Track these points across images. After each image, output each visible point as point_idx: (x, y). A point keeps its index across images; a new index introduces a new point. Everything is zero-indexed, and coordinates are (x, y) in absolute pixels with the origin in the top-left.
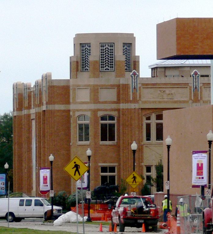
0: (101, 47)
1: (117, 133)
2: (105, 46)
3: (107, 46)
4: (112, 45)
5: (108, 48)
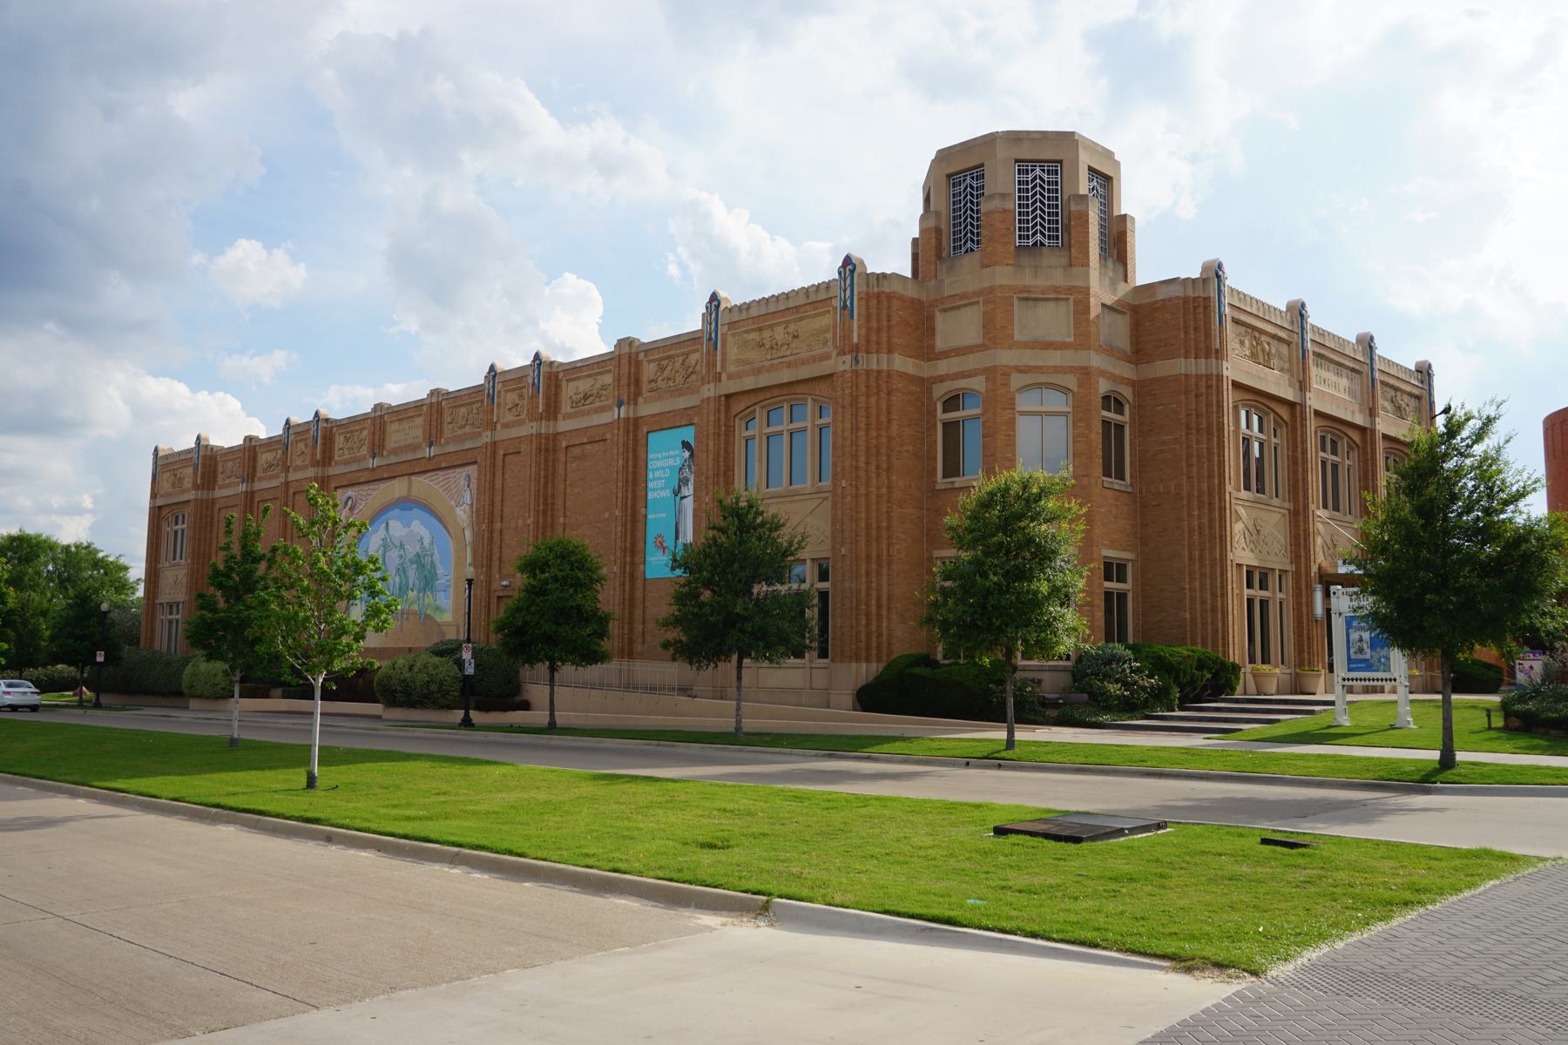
0: (1019, 174)
1: (936, 449)
2: (1032, 170)
3: (968, 180)
5: (1041, 179)
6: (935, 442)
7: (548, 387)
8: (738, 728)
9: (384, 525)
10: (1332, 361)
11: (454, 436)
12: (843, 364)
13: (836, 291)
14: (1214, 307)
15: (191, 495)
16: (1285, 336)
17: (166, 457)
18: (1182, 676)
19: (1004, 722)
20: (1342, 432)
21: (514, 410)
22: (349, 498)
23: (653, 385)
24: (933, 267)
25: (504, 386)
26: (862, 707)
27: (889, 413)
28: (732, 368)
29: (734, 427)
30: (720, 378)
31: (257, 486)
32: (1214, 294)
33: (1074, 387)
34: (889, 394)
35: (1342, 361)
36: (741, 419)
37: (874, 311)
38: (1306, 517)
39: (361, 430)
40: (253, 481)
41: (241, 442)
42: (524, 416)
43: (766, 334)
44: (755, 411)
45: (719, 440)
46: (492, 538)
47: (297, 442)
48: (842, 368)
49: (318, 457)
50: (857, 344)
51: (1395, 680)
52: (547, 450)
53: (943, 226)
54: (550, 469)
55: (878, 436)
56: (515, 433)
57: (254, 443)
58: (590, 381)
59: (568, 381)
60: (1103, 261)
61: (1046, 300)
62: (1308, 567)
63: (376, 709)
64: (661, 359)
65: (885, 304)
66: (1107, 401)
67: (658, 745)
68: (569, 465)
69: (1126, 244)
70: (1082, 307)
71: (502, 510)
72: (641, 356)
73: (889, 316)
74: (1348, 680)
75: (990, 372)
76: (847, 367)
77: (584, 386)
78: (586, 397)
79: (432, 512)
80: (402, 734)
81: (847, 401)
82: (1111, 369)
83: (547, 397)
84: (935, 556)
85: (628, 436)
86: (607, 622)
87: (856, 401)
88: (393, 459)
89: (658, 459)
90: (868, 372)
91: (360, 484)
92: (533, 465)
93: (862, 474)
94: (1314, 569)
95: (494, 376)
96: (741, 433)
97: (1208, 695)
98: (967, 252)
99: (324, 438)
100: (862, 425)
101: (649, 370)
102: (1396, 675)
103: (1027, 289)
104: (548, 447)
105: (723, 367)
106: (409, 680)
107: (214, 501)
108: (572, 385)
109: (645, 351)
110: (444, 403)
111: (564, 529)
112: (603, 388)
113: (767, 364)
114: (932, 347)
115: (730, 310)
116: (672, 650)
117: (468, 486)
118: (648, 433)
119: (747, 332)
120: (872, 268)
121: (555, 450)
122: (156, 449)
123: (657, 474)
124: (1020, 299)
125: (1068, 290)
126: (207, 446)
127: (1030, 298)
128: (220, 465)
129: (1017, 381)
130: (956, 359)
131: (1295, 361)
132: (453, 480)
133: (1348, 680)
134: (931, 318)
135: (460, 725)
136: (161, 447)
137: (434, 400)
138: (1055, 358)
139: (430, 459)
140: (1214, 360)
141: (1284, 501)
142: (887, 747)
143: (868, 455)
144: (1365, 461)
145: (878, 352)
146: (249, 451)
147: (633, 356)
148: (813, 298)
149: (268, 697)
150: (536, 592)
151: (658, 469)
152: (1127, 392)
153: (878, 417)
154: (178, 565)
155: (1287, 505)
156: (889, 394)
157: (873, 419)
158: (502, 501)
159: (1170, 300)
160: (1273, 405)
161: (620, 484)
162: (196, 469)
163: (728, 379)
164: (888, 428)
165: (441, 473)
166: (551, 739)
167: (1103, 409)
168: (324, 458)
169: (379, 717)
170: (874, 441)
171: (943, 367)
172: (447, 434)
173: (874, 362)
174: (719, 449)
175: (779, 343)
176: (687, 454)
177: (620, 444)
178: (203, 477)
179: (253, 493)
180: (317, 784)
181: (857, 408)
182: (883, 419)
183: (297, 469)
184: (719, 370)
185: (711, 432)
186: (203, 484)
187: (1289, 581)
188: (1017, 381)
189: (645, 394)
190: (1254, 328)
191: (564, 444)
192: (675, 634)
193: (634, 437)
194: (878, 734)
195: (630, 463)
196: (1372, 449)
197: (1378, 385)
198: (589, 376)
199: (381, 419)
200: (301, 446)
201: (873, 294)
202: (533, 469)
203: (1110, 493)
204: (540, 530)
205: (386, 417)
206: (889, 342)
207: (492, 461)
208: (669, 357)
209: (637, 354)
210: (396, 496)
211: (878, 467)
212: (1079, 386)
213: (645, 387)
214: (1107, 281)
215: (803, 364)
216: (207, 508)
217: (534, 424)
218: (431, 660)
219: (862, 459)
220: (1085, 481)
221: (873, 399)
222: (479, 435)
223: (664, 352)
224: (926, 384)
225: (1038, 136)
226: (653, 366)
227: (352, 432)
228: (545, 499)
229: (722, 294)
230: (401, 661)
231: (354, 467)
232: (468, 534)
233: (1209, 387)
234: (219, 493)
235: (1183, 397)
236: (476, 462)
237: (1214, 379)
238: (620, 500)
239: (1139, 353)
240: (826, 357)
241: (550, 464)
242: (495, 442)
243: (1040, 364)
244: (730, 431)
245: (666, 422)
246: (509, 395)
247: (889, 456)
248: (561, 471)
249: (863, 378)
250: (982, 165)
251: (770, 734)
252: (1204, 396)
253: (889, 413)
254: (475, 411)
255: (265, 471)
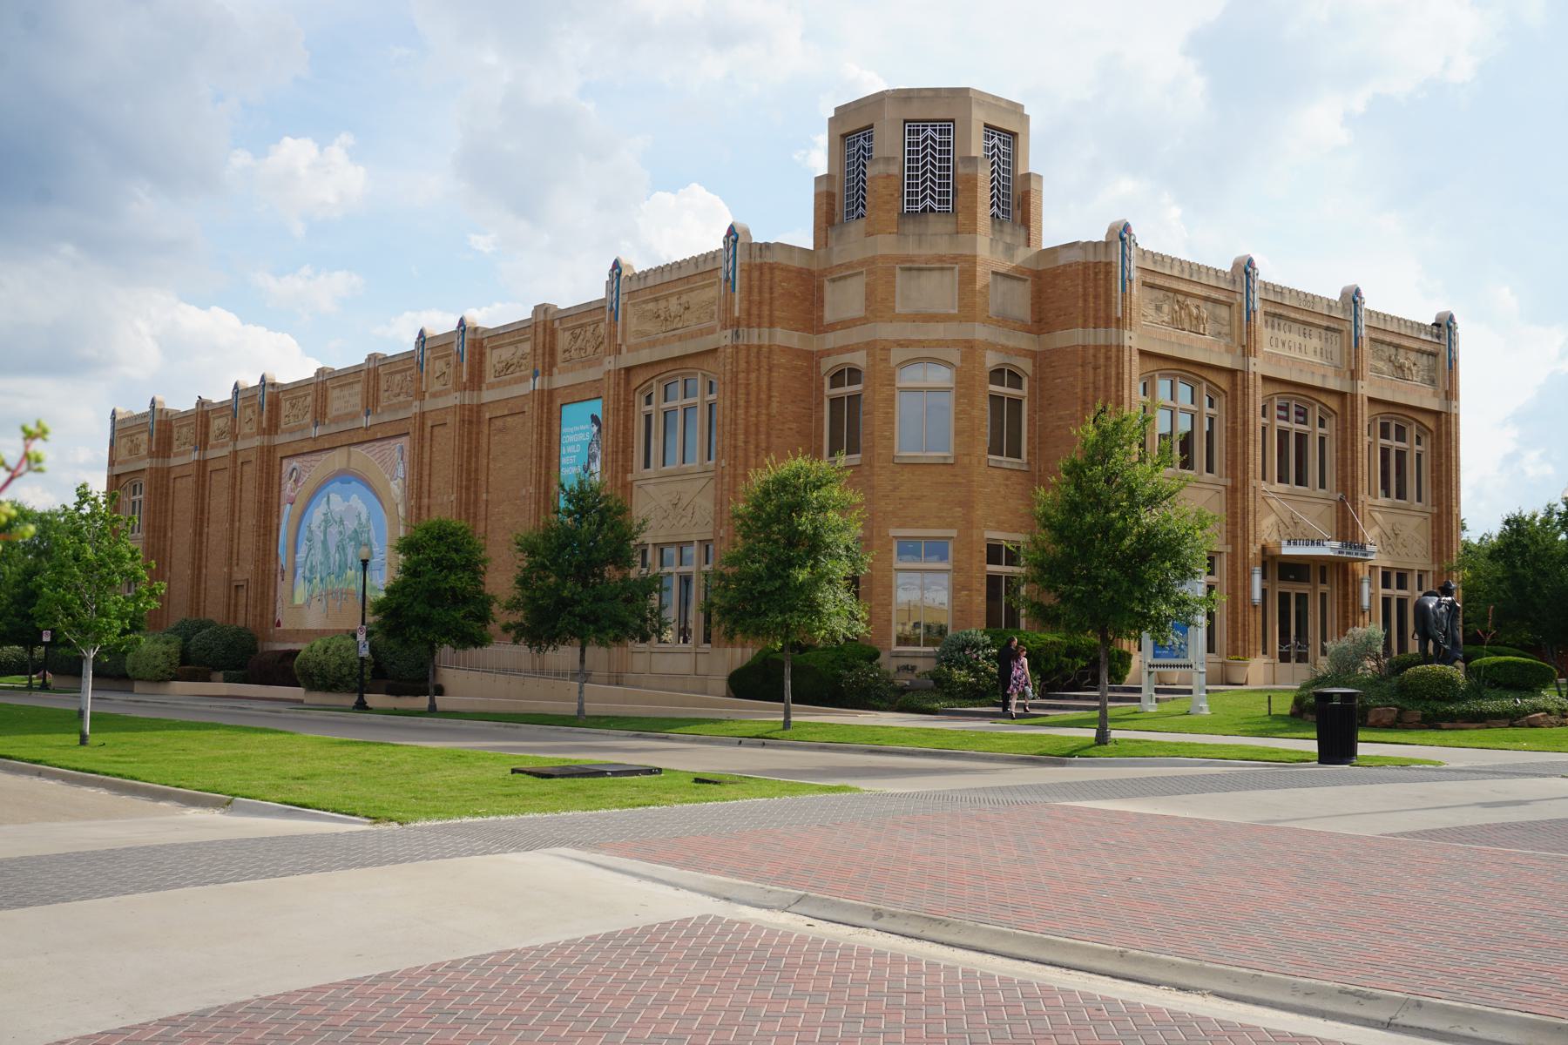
2: (923, 131)
4: (946, 126)
5: (932, 139)
6: (822, 418)
7: (472, 355)
8: (581, 711)
9: (325, 499)
10: (1295, 321)
11: (390, 405)
12: (723, 338)
13: (721, 262)
14: (1116, 273)
15: (145, 464)
16: (1222, 298)
17: (123, 421)
18: (1043, 663)
19: (783, 701)
20: (1314, 399)
21: (441, 379)
22: (294, 469)
23: (567, 354)
24: (824, 233)
25: (432, 353)
26: (733, 692)
27: (769, 389)
28: (632, 341)
29: (634, 401)
30: (620, 350)
31: (211, 454)
32: (1116, 258)
33: (957, 363)
34: (770, 370)
35: (1310, 320)
36: (641, 393)
37: (755, 283)
38: (1245, 494)
39: (305, 396)
40: (205, 449)
41: (194, 407)
42: (449, 386)
43: (662, 304)
44: (652, 386)
45: (618, 415)
46: (420, 514)
47: (245, 407)
48: (724, 342)
49: (154, 449)
50: (738, 318)
51: (1191, 666)
52: (470, 422)
53: (837, 190)
54: (474, 441)
55: (758, 415)
56: (441, 403)
57: (206, 408)
58: (512, 349)
59: (493, 348)
60: (997, 226)
61: (930, 269)
62: (1246, 549)
63: (298, 692)
64: (574, 328)
65: (767, 276)
66: (997, 375)
67: (506, 727)
68: (492, 438)
69: (1029, 205)
70: (968, 277)
71: (429, 486)
72: (557, 323)
73: (771, 289)
74: (1154, 666)
75: (869, 346)
76: (728, 342)
77: (506, 354)
78: (508, 367)
79: (368, 485)
80: (301, 716)
81: (728, 376)
82: (1003, 340)
83: (471, 366)
84: (891, 535)
85: (542, 410)
86: (490, 604)
87: (736, 377)
88: (334, 429)
89: (569, 434)
90: (748, 347)
91: (303, 454)
92: (457, 438)
93: (741, 454)
94: (1254, 549)
95: (423, 343)
96: (641, 408)
97: (1087, 684)
98: (858, 218)
99: (270, 404)
100: (742, 403)
101: (564, 339)
102: (1192, 661)
103: (909, 259)
104: (472, 419)
105: (624, 339)
106: (323, 662)
107: (169, 469)
108: (496, 352)
109: (561, 319)
110: (381, 369)
111: (487, 506)
112: (523, 357)
113: (661, 336)
114: (821, 318)
115: (630, 278)
116: (513, 633)
117: (402, 459)
118: (282, 458)
119: (645, 302)
120: (758, 237)
121: (479, 422)
122: (114, 413)
123: (570, 449)
124: (902, 269)
125: (952, 258)
126: (162, 410)
127: (913, 268)
128: (175, 430)
129: (897, 355)
130: (839, 333)
131: (1236, 323)
132: (388, 452)
133: (1154, 666)
134: (821, 288)
135: (354, 708)
136: (119, 409)
137: (371, 366)
138: (938, 331)
139: (367, 429)
140: (1114, 329)
141: (1221, 477)
142: (690, 729)
143: (746, 432)
144: (1344, 430)
145: (759, 326)
146: (202, 416)
147: (549, 324)
148: (702, 268)
149: (209, 681)
150: (411, 571)
151: (570, 444)
152: (1025, 365)
153: (758, 394)
154: (682, 475)
155: (1223, 481)
156: (770, 370)
157: (753, 398)
158: (430, 475)
159: (1070, 265)
160: (1204, 373)
161: (534, 460)
162: (151, 435)
163: (628, 351)
164: (769, 405)
165: (378, 444)
166: (421, 721)
167: (991, 383)
168: (270, 426)
169: (300, 701)
170: (754, 419)
171: (832, 340)
172: (383, 403)
173: (756, 337)
174: (618, 425)
175: (673, 314)
176: (595, 429)
177: (535, 418)
178: (158, 444)
179: (205, 461)
180: (89, 742)
181: (737, 385)
182: (763, 396)
183: (245, 437)
184: (619, 342)
185: (611, 406)
186: (158, 451)
187: (1222, 564)
188: (897, 355)
189: (560, 365)
190: (1177, 292)
191: (487, 416)
192: (518, 617)
193: (548, 407)
194: (684, 717)
195: (544, 438)
196: (1352, 416)
197: (1366, 344)
198: (511, 344)
199: (324, 384)
200: (249, 411)
201: (756, 265)
202: (457, 443)
203: (998, 472)
204: (463, 507)
205: (328, 382)
206: (771, 315)
207: (421, 431)
208: (581, 326)
209: (553, 321)
210: (337, 468)
211: (757, 446)
212: (962, 361)
213: (560, 357)
214: (1001, 247)
215: (692, 337)
216: (162, 477)
217: (458, 394)
218: (344, 643)
219: (741, 437)
220: (966, 460)
221: (753, 376)
222: (410, 404)
223: (577, 320)
224: (813, 358)
225: (930, 94)
226: (567, 334)
227: (296, 398)
228: (469, 474)
229: (624, 261)
230: (318, 643)
231: (298, 436)
232: (401, 510)
233: (1108, 358)
234: (175, 461)
235: (1079, 370)
236: (408, 434)
237: (1114, 350)
238: (534, 476)
239: (1040, 323)
240: (712, 331)
241: (474, 436)
242: (424, 413)
243: (922, 337)
244: (629, 405)
245: (578, 394)
246: (437, 362)
247: (768, 435)
248: (484, 441)
249: (742, 354)
250: (871, 126)
251: (608, 717)
252: (1103, 368)
253: (769, 389)
254: (409, 378)
255: (217, 438)
